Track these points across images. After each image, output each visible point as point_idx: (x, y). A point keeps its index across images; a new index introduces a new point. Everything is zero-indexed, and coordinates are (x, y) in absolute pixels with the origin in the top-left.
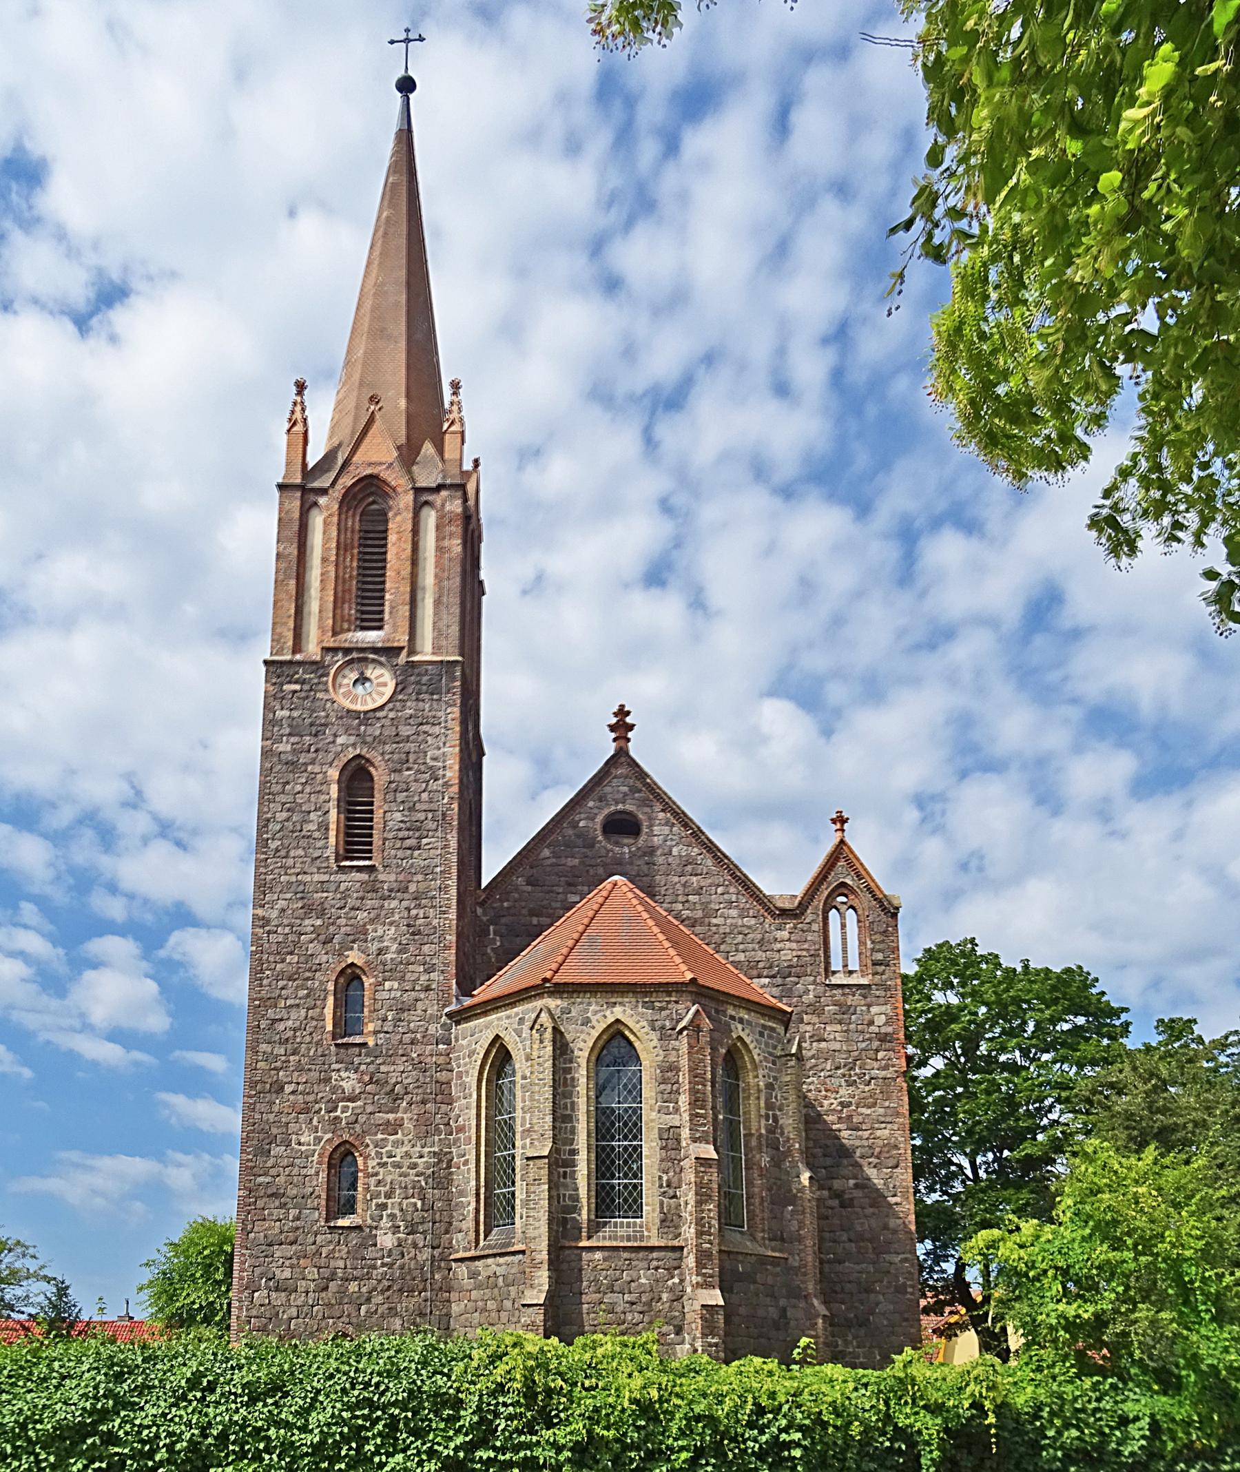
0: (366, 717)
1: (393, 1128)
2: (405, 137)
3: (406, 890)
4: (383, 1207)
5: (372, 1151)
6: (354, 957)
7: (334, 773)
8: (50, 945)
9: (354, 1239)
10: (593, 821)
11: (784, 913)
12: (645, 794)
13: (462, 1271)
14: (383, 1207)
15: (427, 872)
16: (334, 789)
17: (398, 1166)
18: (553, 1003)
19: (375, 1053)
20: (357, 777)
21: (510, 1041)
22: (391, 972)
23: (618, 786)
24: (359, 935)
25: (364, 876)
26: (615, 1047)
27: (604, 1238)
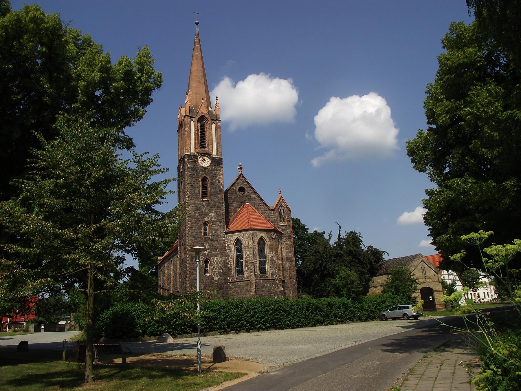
0: (206, 168)
1: (216, 255)
2: (340, 231)
3: (215, 206)
4: (215, 272)
5: (212, 260)
6: (206, 219)
7: (200, 180)
8: (368, 241)
9: (210, 278)
10: (236, 189)
11: (272, 210)
12: (246, 183)
13: (231, 285)
14: (215, 272)
15: (219, 202)
16: (200, 183)
17: (217, 263)
18: (251, 232)
19: (211, 240)
20: (204, 180)
21: (241, 238)
22: (213, 223)
23: (241, 181)
24: (207, 215)
25: (207, 202)
26: (238, 241)
27: (45, 369)
